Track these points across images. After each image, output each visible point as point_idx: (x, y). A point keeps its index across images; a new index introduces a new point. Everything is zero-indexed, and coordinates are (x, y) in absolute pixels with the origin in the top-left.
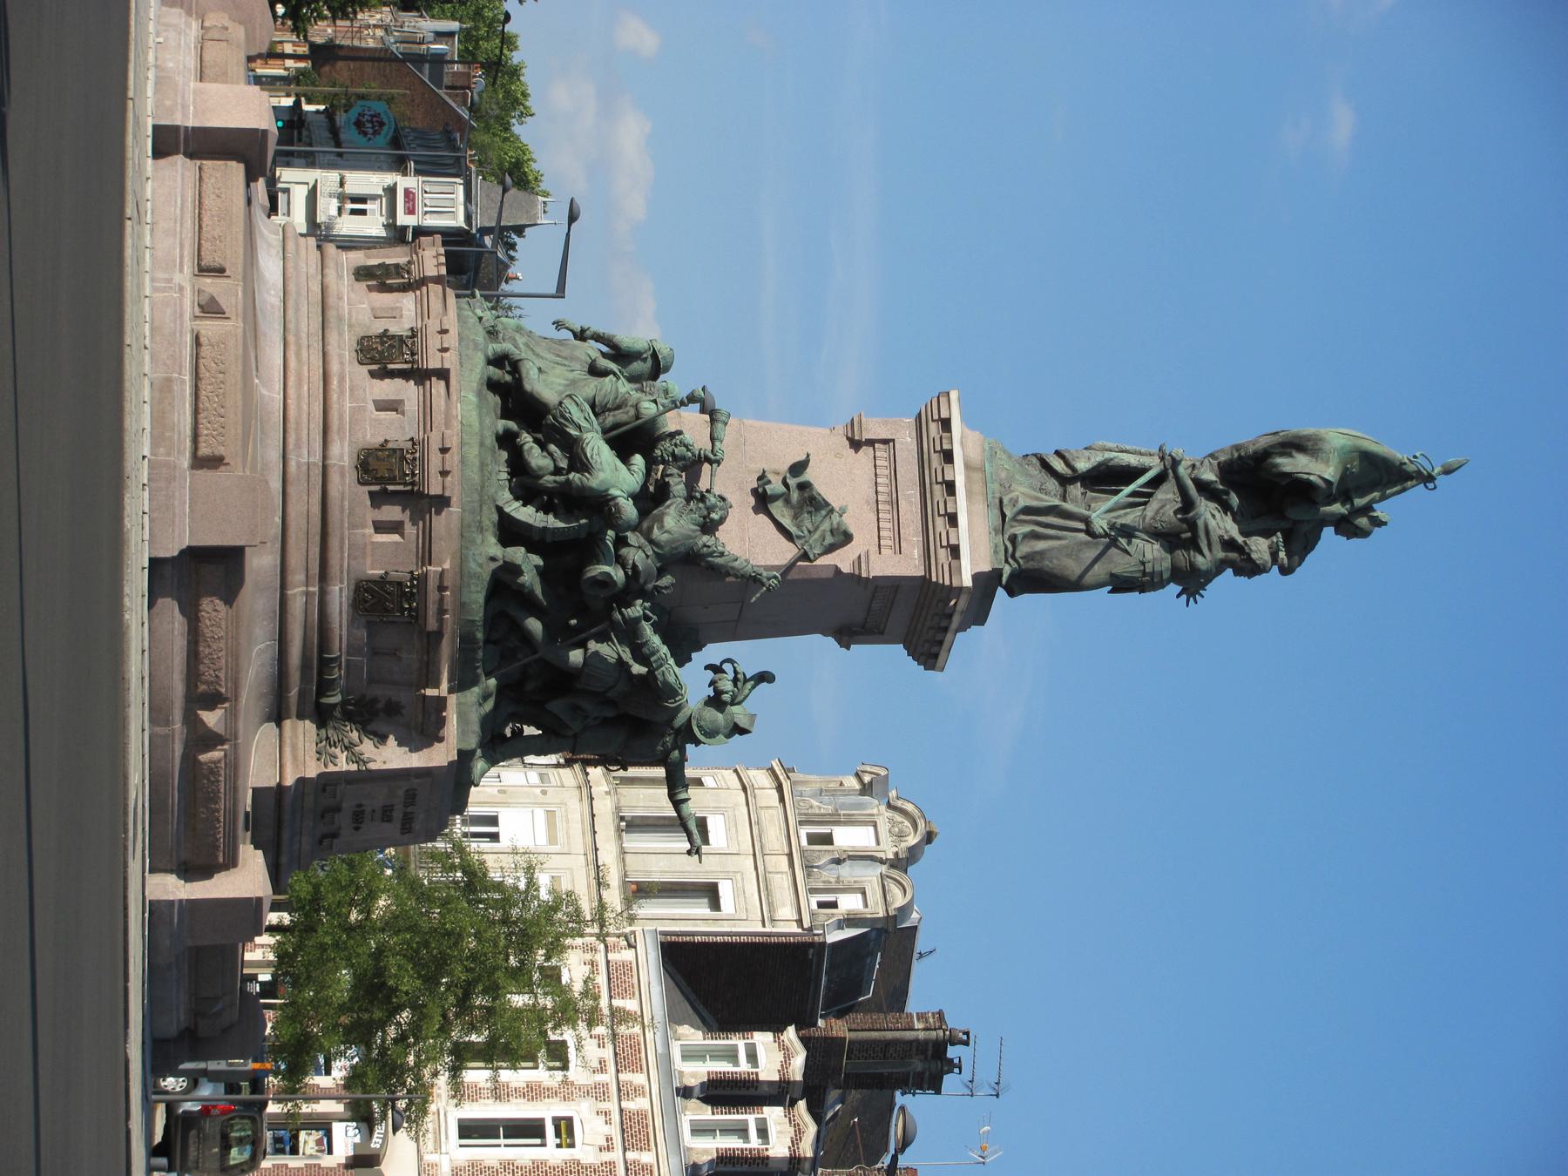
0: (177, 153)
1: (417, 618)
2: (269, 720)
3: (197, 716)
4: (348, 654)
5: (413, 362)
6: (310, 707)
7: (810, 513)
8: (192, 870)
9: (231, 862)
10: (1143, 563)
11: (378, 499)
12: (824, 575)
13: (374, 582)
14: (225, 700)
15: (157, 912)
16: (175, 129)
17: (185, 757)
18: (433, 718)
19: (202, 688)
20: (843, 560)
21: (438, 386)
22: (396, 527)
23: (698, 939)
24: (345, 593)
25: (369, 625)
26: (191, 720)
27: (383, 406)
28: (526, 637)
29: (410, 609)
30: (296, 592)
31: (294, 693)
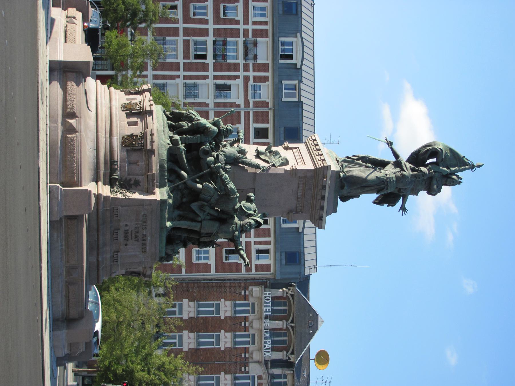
0: (60, 7)
1: (144, 146)
2: (93, 181)
3: (66, 121)
4: (120, 162)
6: (108, 180)
7: (274, 156)
10: (386, 175)
11: (128, 116)
12: (281, 172)
13: (129, 136)
14: (77, 117)
17: (62, 137)
18: (151, 184)
19: (68, 110)
20: (288, 168)
21: (150, 119)
22: (135, 124)
24: (119, 140)
25: (128, 151)
26: (64, 123)
28: (181, 177)
29: (141, 143)
30: (102, 140)
31: (102, 172)
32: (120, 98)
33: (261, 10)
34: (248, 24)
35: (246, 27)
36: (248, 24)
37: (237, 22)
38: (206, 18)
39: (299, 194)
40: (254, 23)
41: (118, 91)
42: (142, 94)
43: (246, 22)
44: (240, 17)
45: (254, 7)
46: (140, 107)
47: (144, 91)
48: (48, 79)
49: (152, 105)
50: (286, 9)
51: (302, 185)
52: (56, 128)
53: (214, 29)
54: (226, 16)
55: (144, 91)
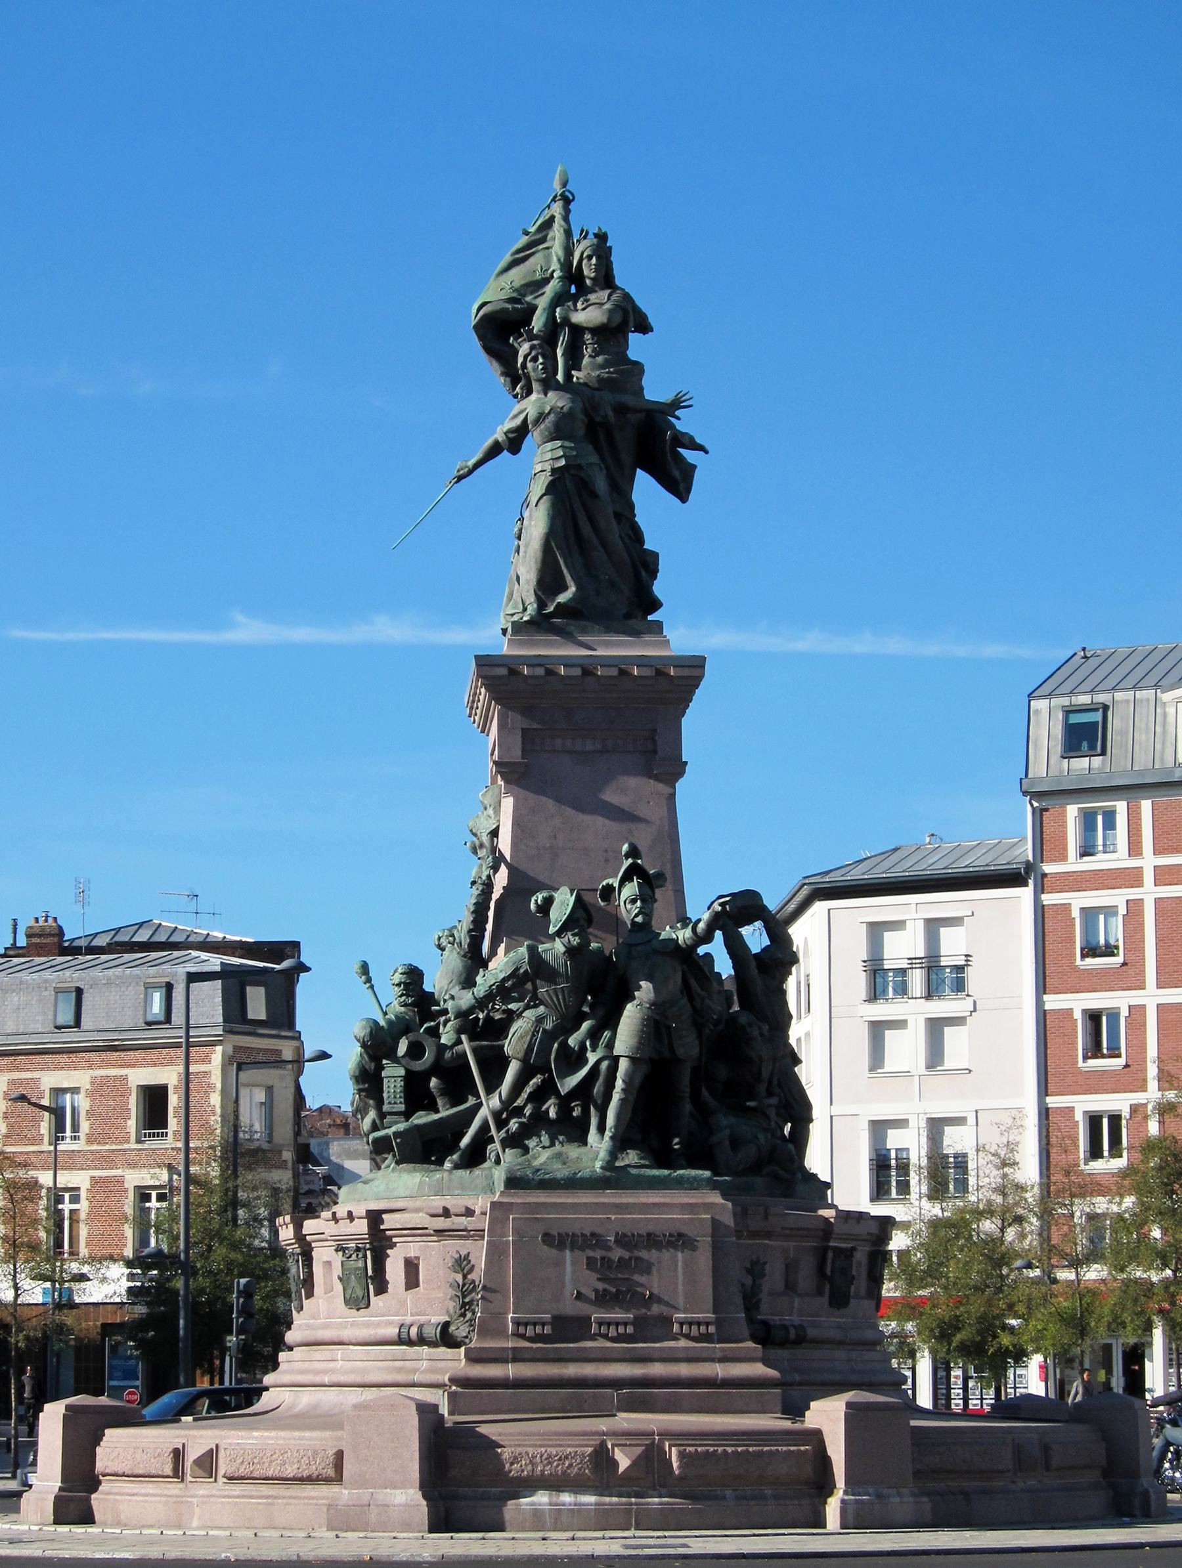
0: (89, 1499)
5: (366, 1250)
8: (824, 1486)
9: (816, 1437)
14: (603, 1444)
15: (854, 1520)
16: (58, 1501)
21: (389, 1221)
22: (411, 1267)
23: (838, 884)
27: (412, 1281)
32: (320, 1313)
33: (1095, 829)
34: (1139, 871)
35: (1149, 877)
36: (1139, 871)
37: (1134, 908)
38: (1124, 1013)
39: (589, 746)
40: (1135, 848)
41: (298, 1319)
42: (309, 1244)
43: (1132, 878)
44: (1117, 898)
45: (1083, 855)
46: (358, 1249)
47: (300, 1238)
48: (480, 1535)
49: (334, 1214)
50: (1085, 745)
51: (558, 742)
52: (578, 1511)
53: (1159, 987)
54: (1117, 947)
55: (300, 1238)
